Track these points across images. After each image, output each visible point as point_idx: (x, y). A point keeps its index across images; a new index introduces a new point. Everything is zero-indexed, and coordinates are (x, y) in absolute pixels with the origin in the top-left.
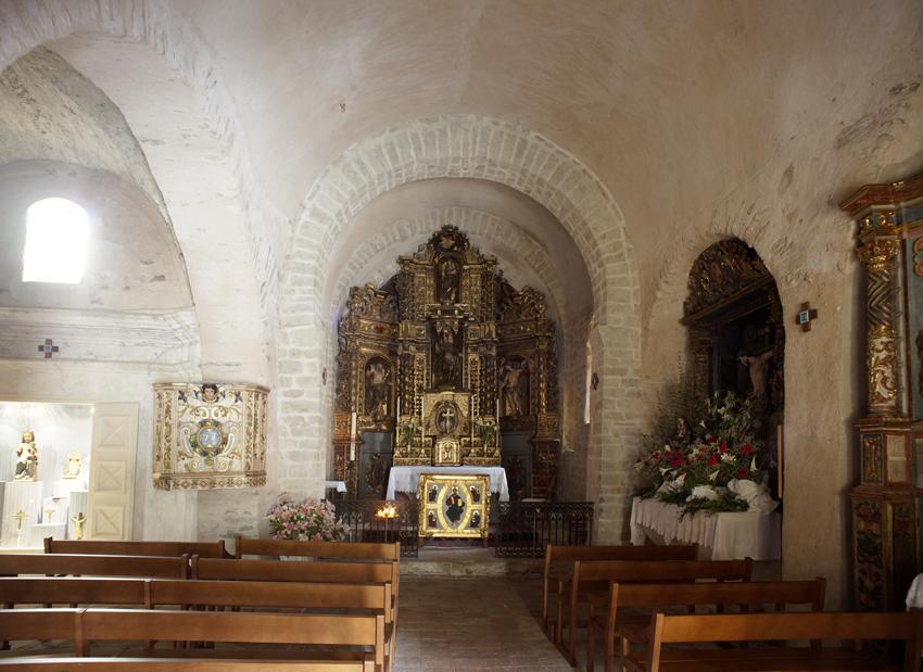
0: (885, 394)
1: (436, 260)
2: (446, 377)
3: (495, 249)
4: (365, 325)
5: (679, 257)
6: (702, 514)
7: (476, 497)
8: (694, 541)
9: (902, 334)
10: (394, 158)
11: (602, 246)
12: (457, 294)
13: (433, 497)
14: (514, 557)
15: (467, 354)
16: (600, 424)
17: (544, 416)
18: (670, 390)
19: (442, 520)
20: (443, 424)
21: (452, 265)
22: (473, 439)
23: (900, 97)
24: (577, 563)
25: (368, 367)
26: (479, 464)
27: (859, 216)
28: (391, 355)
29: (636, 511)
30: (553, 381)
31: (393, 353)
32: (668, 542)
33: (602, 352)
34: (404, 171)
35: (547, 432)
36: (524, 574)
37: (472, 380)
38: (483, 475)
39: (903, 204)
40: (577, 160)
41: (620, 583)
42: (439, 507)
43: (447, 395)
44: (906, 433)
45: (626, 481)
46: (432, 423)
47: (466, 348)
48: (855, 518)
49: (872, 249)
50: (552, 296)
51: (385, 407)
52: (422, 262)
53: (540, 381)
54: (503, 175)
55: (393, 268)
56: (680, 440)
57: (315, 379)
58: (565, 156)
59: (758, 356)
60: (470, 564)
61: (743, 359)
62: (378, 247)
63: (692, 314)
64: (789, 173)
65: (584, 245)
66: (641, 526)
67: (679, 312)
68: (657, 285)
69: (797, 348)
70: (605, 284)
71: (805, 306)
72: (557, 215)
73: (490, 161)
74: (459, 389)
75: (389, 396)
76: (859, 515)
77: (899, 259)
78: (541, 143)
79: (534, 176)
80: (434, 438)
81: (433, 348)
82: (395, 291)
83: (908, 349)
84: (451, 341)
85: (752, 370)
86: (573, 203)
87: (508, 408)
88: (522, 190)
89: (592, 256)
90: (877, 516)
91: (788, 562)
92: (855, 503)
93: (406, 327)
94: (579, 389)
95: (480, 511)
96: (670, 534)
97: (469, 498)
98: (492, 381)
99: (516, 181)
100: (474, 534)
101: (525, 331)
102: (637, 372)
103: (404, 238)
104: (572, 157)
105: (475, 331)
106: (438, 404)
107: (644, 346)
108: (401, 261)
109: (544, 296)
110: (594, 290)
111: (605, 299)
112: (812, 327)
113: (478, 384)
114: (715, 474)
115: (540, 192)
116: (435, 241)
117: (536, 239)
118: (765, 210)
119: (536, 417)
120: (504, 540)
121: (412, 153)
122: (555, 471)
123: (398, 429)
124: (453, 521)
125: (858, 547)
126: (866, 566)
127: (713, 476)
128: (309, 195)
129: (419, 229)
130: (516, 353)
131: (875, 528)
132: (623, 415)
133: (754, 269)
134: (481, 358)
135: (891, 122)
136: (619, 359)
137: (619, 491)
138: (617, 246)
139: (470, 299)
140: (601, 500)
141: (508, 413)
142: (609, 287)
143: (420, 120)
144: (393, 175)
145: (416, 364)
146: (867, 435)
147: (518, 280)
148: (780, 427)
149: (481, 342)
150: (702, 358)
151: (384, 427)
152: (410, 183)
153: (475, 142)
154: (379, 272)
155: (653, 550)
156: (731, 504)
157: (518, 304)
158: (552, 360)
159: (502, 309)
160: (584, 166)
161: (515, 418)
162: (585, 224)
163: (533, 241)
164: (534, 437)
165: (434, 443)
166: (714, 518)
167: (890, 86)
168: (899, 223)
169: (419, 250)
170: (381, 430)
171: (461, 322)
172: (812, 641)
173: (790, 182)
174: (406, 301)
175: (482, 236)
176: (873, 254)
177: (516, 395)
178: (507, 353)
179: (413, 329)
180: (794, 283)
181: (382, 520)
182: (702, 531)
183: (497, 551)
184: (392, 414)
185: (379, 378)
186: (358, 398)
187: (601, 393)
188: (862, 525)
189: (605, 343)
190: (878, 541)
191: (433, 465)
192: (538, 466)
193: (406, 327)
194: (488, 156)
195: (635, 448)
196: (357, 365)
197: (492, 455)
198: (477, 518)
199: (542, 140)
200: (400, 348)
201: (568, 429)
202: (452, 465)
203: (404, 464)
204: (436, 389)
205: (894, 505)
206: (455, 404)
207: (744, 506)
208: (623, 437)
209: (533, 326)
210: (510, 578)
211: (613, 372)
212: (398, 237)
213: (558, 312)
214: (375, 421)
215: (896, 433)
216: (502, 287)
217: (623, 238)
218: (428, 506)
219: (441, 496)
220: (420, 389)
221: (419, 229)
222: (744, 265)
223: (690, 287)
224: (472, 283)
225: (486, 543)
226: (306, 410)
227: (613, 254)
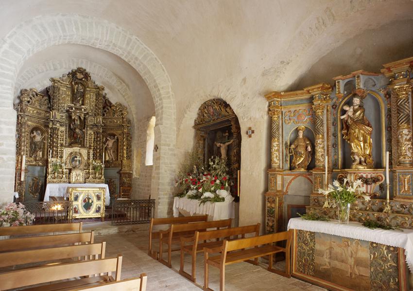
0: (277, 161)
1: (73, 83)
2: (75, 139)
3: (103, 83)
4: (30, 110)
5: (196, 102)
6: (208, 203)
7: (99, 198)
8: (204, 214)
9: (281, 142)
10: (64, 30)
11: (162, 91)
12: (83, 101)
13: (76, 198)
14: (120, 225)
15: (87, 130)
16: (159, 166)
17: (125, 161)
18: (186, 154)
19: (81, 209)
20: (74, 163)
21: (80, 87)
22: (91, 171)
23: (283, 65)
24: (173, 225)
25: (32, 132)
26: (94, 182)
27: (270, 101)
28: (45, 126)
29: (176, 202)
30: (129, 146)
31: (47, 126)
32: (192, 215)
33: (161, 136)
34: (68, 37)
35: (126, 169)
36: (126, 232)
37: (89, 143)
38: (102, 188)
39: (283, 100)
40: (153, 53)
41: (200, 232)
42: (79, 204)
43: (76, 149)
44: (282, 174)
45: (169, 191)
46: (68, 162)
47: (87, 128)
48: (267, 202)
49: (274, 113)
50: (130, 108)
51: (41, 153)
52: (64, 83)
53: (124, 146)
54: (119, 52)
55: (48, 84)
56: (195, 174)
57: (12, 137)
58: (148, 50)
59: (224, 143)
60: (100, 230)
61: (218, 145)
62: (40, 71)
63: (198, 125)
64: (244, 80)
65: (153, 91)
66: (178, 209)
67: (193, 124)
68: (185, 111)
69: (245, 142)
70: (162, 108)
71: (250, 128)
72: (141, 75)
73: (114, 44)
74: (83, 146)
75: (44, 148)
76: (269, 201)
77: (281, 117)
78: (138, 42)
79: (133, 55)
80: (70, 170)
81: (70, 126)
82: (49, 95)
83: (282, 146)
84: (79, 123)
85: (221, 149)
86: (151, 71)
87: (107, 157)
88: (126, 60)
89: (157, 95)
90: (274, 201)
91: (241, 219)
92: (267, 197)
93: (55, 113)
94: (142, 150)
95: (101, 205)
96: (193, 211)
97: (95, 199)
98: (100, 144)
99: (125, 55)
100: (98, 215)
101: (117, 122)
102: (174, 145)
103: (55, 69)
104: (151, 51)
105: (90, 121)
106: (71, 153)
107: (178, 135)
108: (53, 80)
109: (126, 108)
110: (156, 109)
111: (162, 114)
112: (252, 136)
113: (92, 145)
114: (213, 188)
115: (135, 63)
116: (73, 74)
117: (124, 82)
118: (235, 91)
119: (122, 161)
120: (116, 217)
121: (74, 30)
122: (130, 186)
123: (49, 165)
124: (87, 210)
125: (267, 212)
126: (269, 218)
127: (212, 189)
128: (8, 35)
129: (64, 66)
130: (112, 132)
131: (273, 205)
132: (168, 162)
133: (226, 111)
134: (94, 133)
135: (281, 73)
136: (167, 140)
137: (166, 194)
138: (168, 93)
139: (90, 102)
140: (159, 198)
141: (107, 160)
142: (164, 109)
143: (79, 15)
144: (62, 38)
145: (59, 133)
146: (271, 175)
147: (113, 99)
148: (239, 171)
149: (95, 125)
150: (201, 142)
151: (40, 164)
152: (69, 44)
153: (107, 33)
154: (40, 84)
155: (183, 219)
156: (218, 199)
157: (114, 110)
158: (129, 137)
159: (105, 111)
160: (155, 56)
161: (111, 162)
162: (155, 81)
163: (122, 83)
164: (121, 170)
165: (69, 174)
166: (213, 204)
167: (281, 60)
168: (281, 106)
169: (63, 77)
170: (39, 165)
171: (85, 115)
172: (255, 247)
173: (245, 83)
174: (55, 101)
175: (98, 76)
176: (274, 114)
177: (112, 151)
178: (106, 132)
179: (58, 115)
180: (245, 120)
181: (53, 212)
182: (208, 209)
183: (112, 222)
184: (45, 157)
185: (38, 138)
186: (25, 148)
187: (159, 153)
188: (269, 205)
189: (162, 132)
190: (274, 210)
191: (69, 183)
192: (122, 184)
193: (55, 113)
194: (113, 41)
195: (173, 177)
196: (26, 130)
197: (100, 178)
198: (99, 208)
199: (138, 41)
200: (51, 124)
201: (136, 167)
202: (80, 183)
203: (53, 182)
204: (70, 145)
205: (279, 198)
206: (80, 154)
207: (223, 199)
208: (168, 172)
209: (121, 121)
210: (120, 234)
211: (165, 145)
212: (52, 68)
213: (132, 115)
214: (36, 160)
215: (279, 174)
216: (106, 100)
217: (170, 90)
218: (75, 203)
219: (81, 199)
220: (62, 145)
221: (64, 66)
222: (222, 110)
223: (199, 114)
224: (91, 98)
225: (103, 219)
226: (5, 154)
227: (166, 96)
